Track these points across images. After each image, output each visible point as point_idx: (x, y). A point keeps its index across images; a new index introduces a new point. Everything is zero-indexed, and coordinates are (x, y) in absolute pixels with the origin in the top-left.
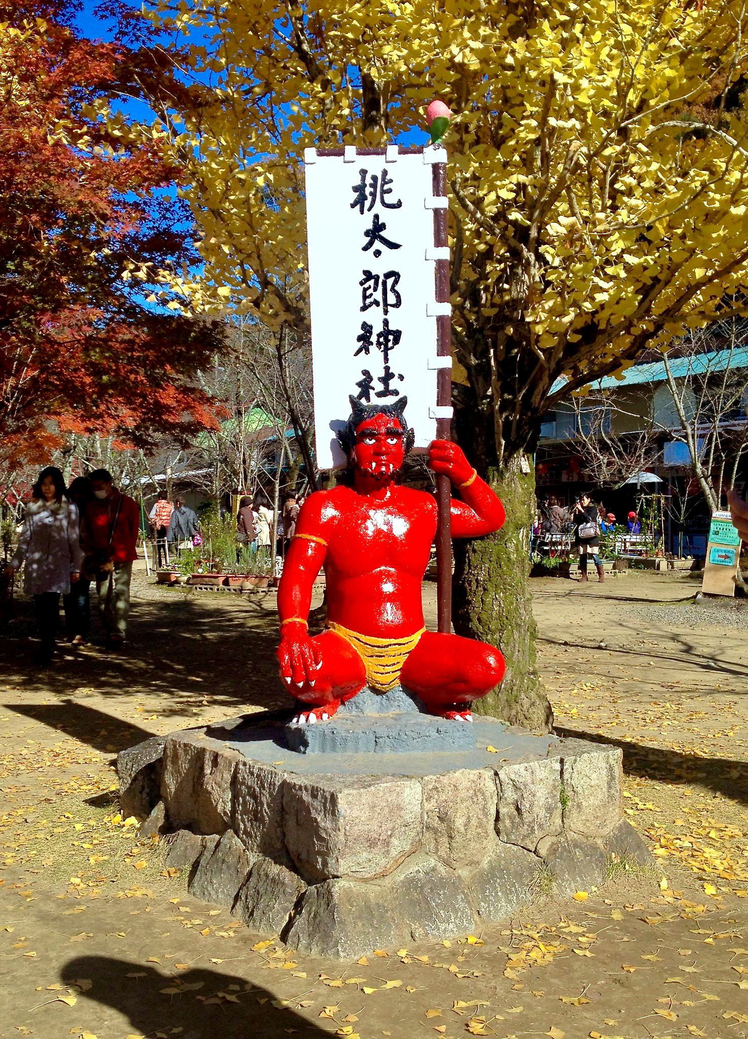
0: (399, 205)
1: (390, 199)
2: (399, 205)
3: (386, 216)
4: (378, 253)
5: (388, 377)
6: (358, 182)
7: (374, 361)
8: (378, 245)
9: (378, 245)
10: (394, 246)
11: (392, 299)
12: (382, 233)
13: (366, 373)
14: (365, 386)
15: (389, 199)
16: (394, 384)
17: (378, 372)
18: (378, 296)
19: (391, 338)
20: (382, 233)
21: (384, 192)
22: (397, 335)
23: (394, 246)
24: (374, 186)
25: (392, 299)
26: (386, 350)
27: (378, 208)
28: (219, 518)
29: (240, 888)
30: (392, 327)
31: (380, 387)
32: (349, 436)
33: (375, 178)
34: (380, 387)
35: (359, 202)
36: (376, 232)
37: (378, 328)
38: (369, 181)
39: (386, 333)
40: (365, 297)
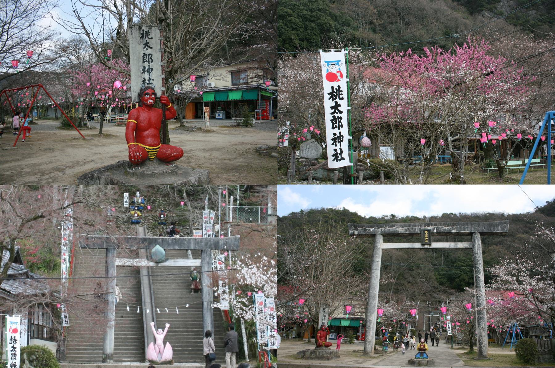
0: (152, 38)
1: (150, 37)
2: (152, 38)
3: (148, 40)
4: (147, 49)
5: (149, 80)
6: (331, 91)
7: (146, 76)
8: (147, 47)
9: (147, 47)
10: (151, 48)
11: (150, 60)
12: (339, 108)
13: (144, 78)
14: (144, 81)
15: (341, 96)
16: (151, 81)
17: (147, 78)
18: (147, 60)
19: (150, 70)
20: (339, 108)
21: (339, 94)
22: (152, 69)
23: (151, 48)
24: (146, 33)
25: (150, 60)
26: (149, 73)
27: (338, 100)
28: (182, 164)
29: (65, 208)
30: (151, 67)
31: (147, 82)
32: (141, 95)
33: (336, 89)
34: (147, 82)
35: (142, 37)
36: (146, 44)
37: (147, 68)
38: (335, 90)
39: (149, 68)
40: (144, 60)
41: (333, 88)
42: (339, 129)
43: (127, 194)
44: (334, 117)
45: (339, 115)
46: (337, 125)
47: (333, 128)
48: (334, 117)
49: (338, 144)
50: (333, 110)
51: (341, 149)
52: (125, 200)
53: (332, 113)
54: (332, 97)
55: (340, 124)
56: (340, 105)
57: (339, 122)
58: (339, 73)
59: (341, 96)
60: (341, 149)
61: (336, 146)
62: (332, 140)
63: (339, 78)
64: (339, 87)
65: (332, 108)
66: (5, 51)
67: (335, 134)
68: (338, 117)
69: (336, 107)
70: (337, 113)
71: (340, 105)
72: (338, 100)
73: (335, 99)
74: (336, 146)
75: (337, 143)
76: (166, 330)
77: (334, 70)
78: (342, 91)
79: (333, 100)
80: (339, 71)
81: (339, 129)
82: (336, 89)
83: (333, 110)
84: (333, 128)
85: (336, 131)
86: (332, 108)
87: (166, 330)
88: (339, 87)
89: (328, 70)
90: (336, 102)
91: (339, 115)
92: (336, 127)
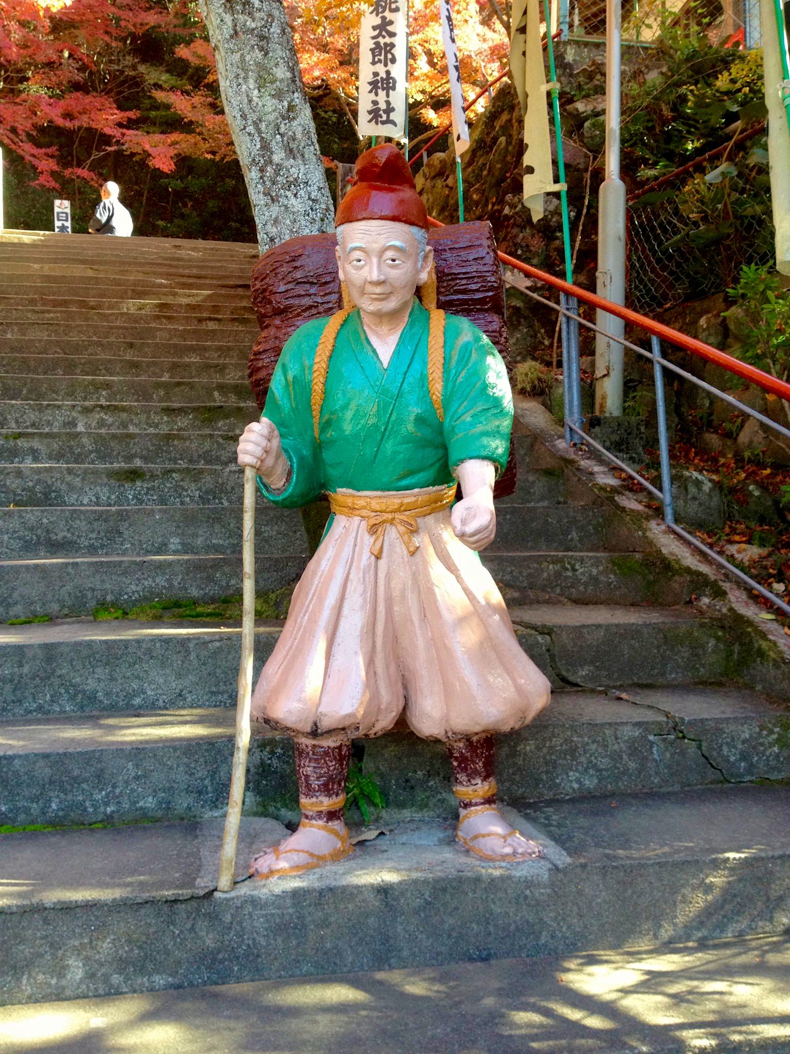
12: (389, 28)
20: (389, 28)
42: (386, 65)
43: (67, 203)
44: (377, 44)
46: (382, 57)
47: (374, 63)
48: (377, 44)
49: (382, 94)
50: (377, 32)
51: (388, 103)
53: (373, 38)
55: (389, 56)
57: (390, 51)
59: (393, 6)
60: (388, 103)
61: (377, 94)
62: (370, 83)
65: (374, 28)
67: (376, 74)
68: (385, 44)
70: (384, 37)
71: (391, 23)
72: (387, 14)
73: (383, 11)
74: (377, 94)
75: (380, 91)
79: (377, 15)
81: (386, 65)
83: (377, 32)
84: (374, 63)
85: (381, 69)
86: (374, 28)
90: (384, 18)
91: (388, 40)
92: (380, 61)
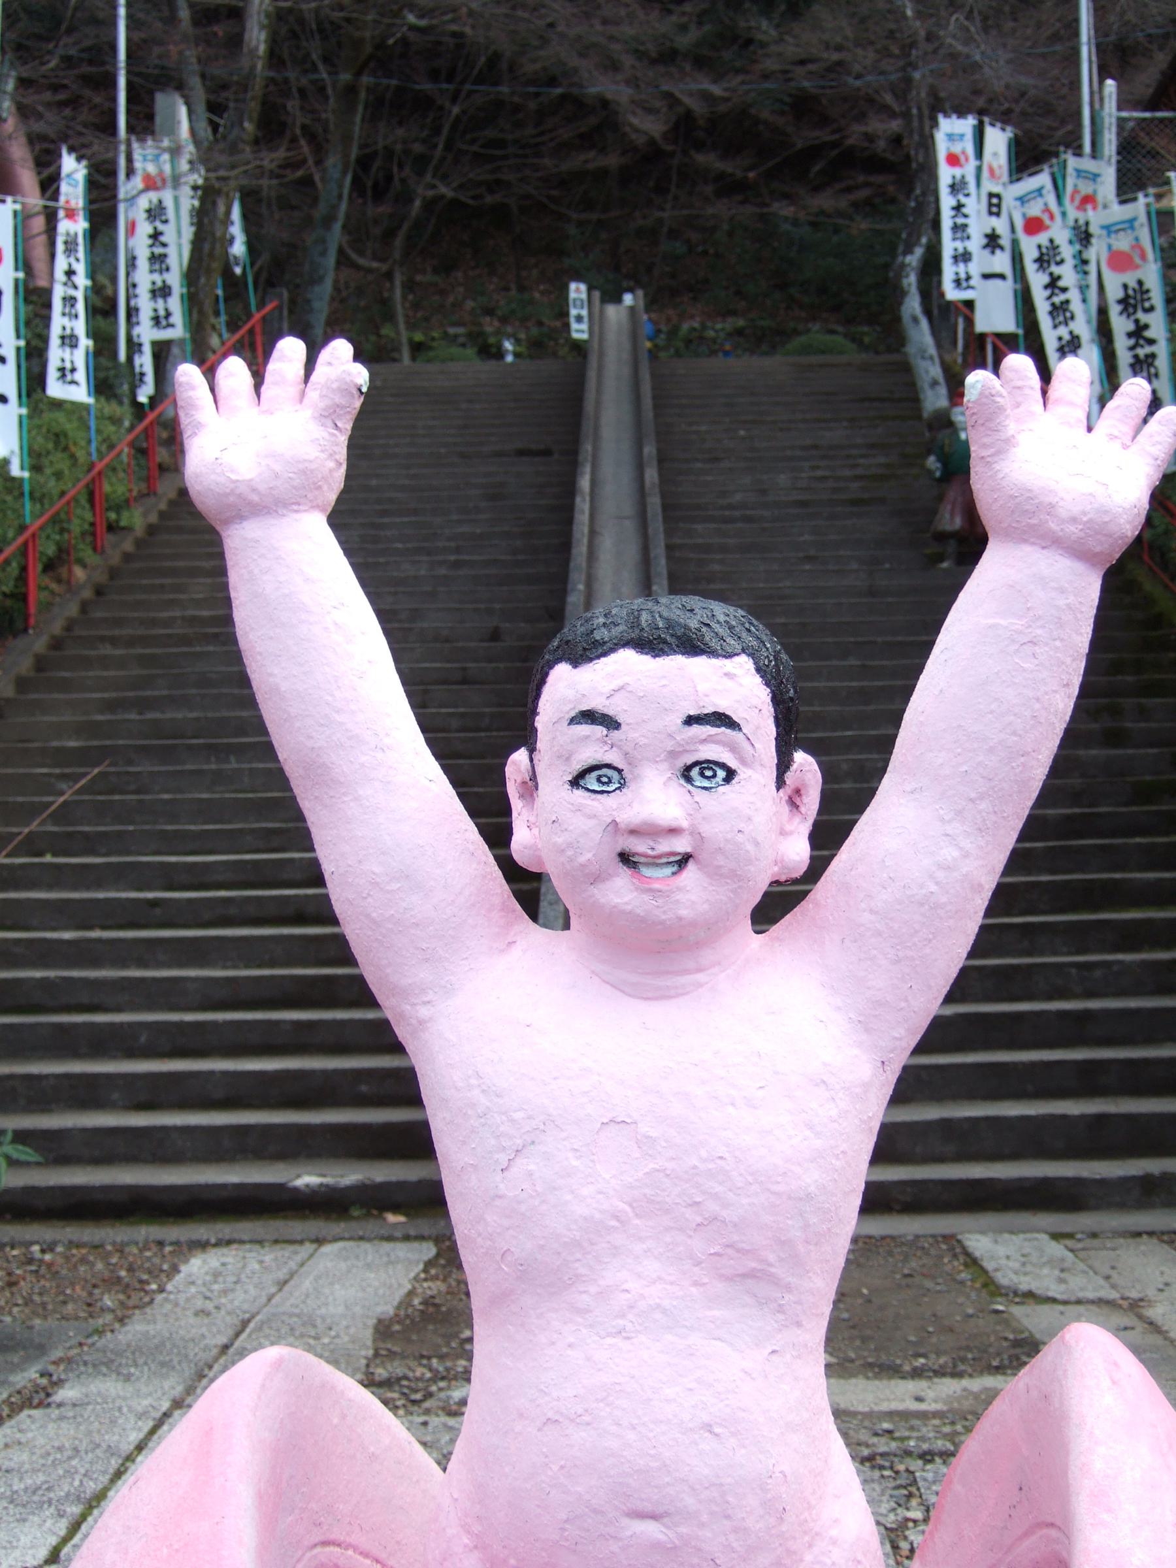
21: (1143, 300)
33: (1134, 290)
41: (1125, 287)
45: (1148, 350)
47: (1055, 327)
52: (573, 312)
54: (1041, 266)
56: (1146, 327)
58: (1138, 251)
59: (1147, 305)
63: (1137, 260)
64: (1140, 283)
65: (1046, 287)
66: (1174, 1380)
69: (1053, 284)
71: (1146, 327)
72: (1140, 315)
73: (1135, 312)
76: (1004, 668)
77: (957, 149)
78: (1148, 291)
80: (963, 153)
82: (1134, 290)
84: (1055, 327)
85: (1063, 331)
87: (1004, 668)
88: (1140, 283)
89: (1110, 247)
90: (1137, 321)
91: (1148, 350)
